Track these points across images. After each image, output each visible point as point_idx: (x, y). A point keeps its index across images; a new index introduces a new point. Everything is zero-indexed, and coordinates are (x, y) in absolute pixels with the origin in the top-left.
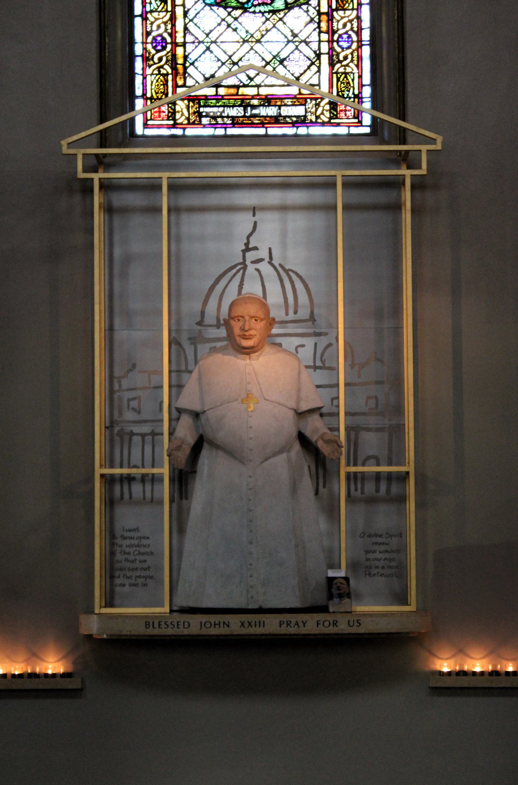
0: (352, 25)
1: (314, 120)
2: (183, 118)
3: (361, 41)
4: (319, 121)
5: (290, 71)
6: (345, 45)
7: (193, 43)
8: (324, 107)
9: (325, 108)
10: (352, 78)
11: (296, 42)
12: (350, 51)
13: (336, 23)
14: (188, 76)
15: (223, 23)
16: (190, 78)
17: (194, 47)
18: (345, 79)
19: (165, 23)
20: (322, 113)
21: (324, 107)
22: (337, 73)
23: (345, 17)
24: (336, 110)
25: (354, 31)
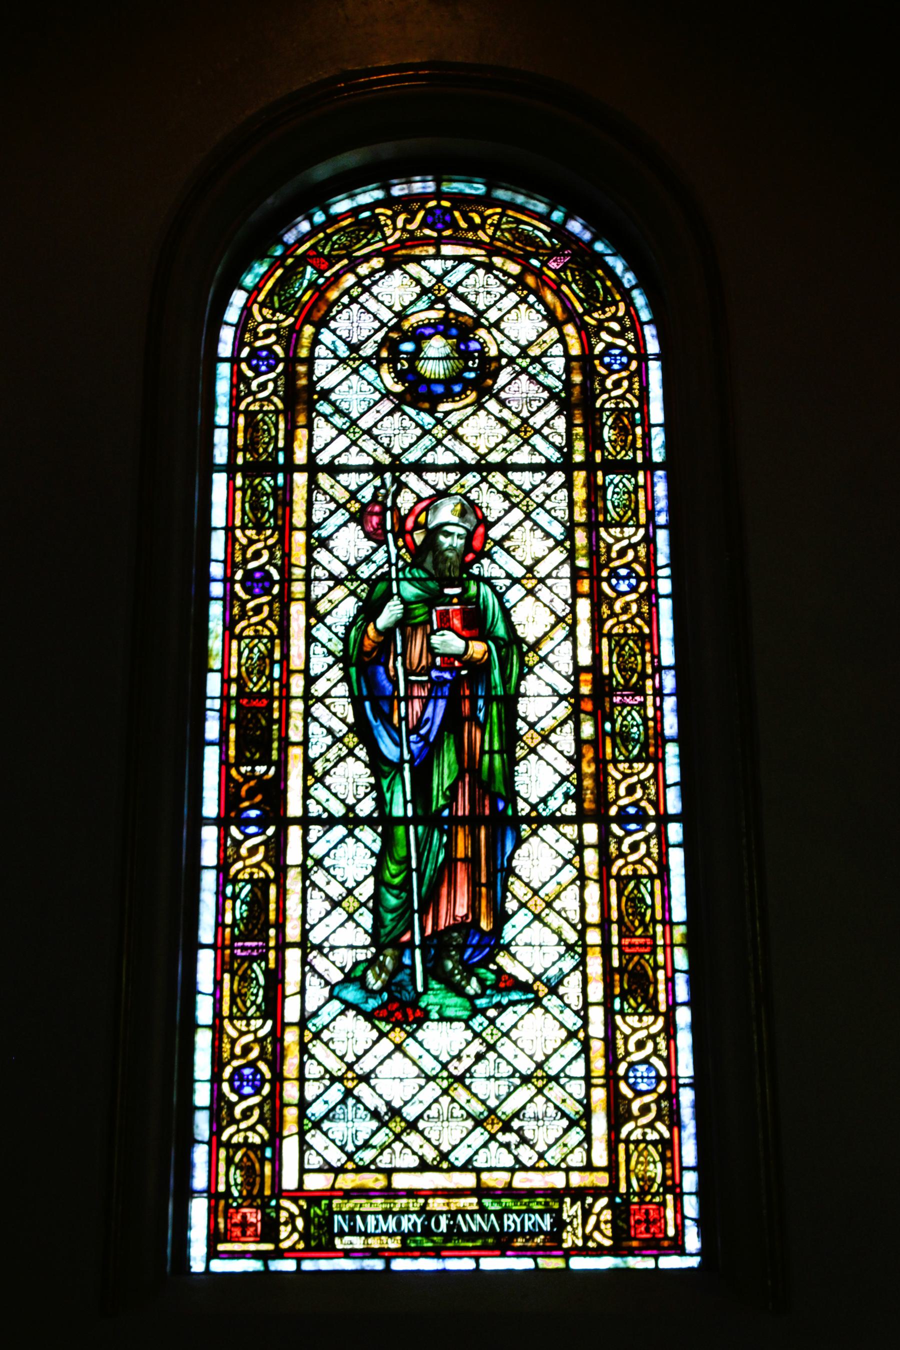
0: (656, 1044)
1: (580, 1243)
2: (296, 1236)
3: (677, 1078)
4: (591, 1244)
5: (526, 1051)
6: (623, 587)
7: (332, 948)
8: (599, 1215)
9: (602, 1218)
10: (649, 889)
11: (542, 1078)
12: (654, 1096)
13: (614, 787)
14: (309, 971)
15: (404, 1137)
16: (313, 976)
17: (331, 939)
18: (636, 892)
19: (270, 548)
20: (597, 1227)
21: (599, 1215)
22: (627, 1141)
23: (641, 1028)
24: (627, 1221)
25: (660, 1057)
